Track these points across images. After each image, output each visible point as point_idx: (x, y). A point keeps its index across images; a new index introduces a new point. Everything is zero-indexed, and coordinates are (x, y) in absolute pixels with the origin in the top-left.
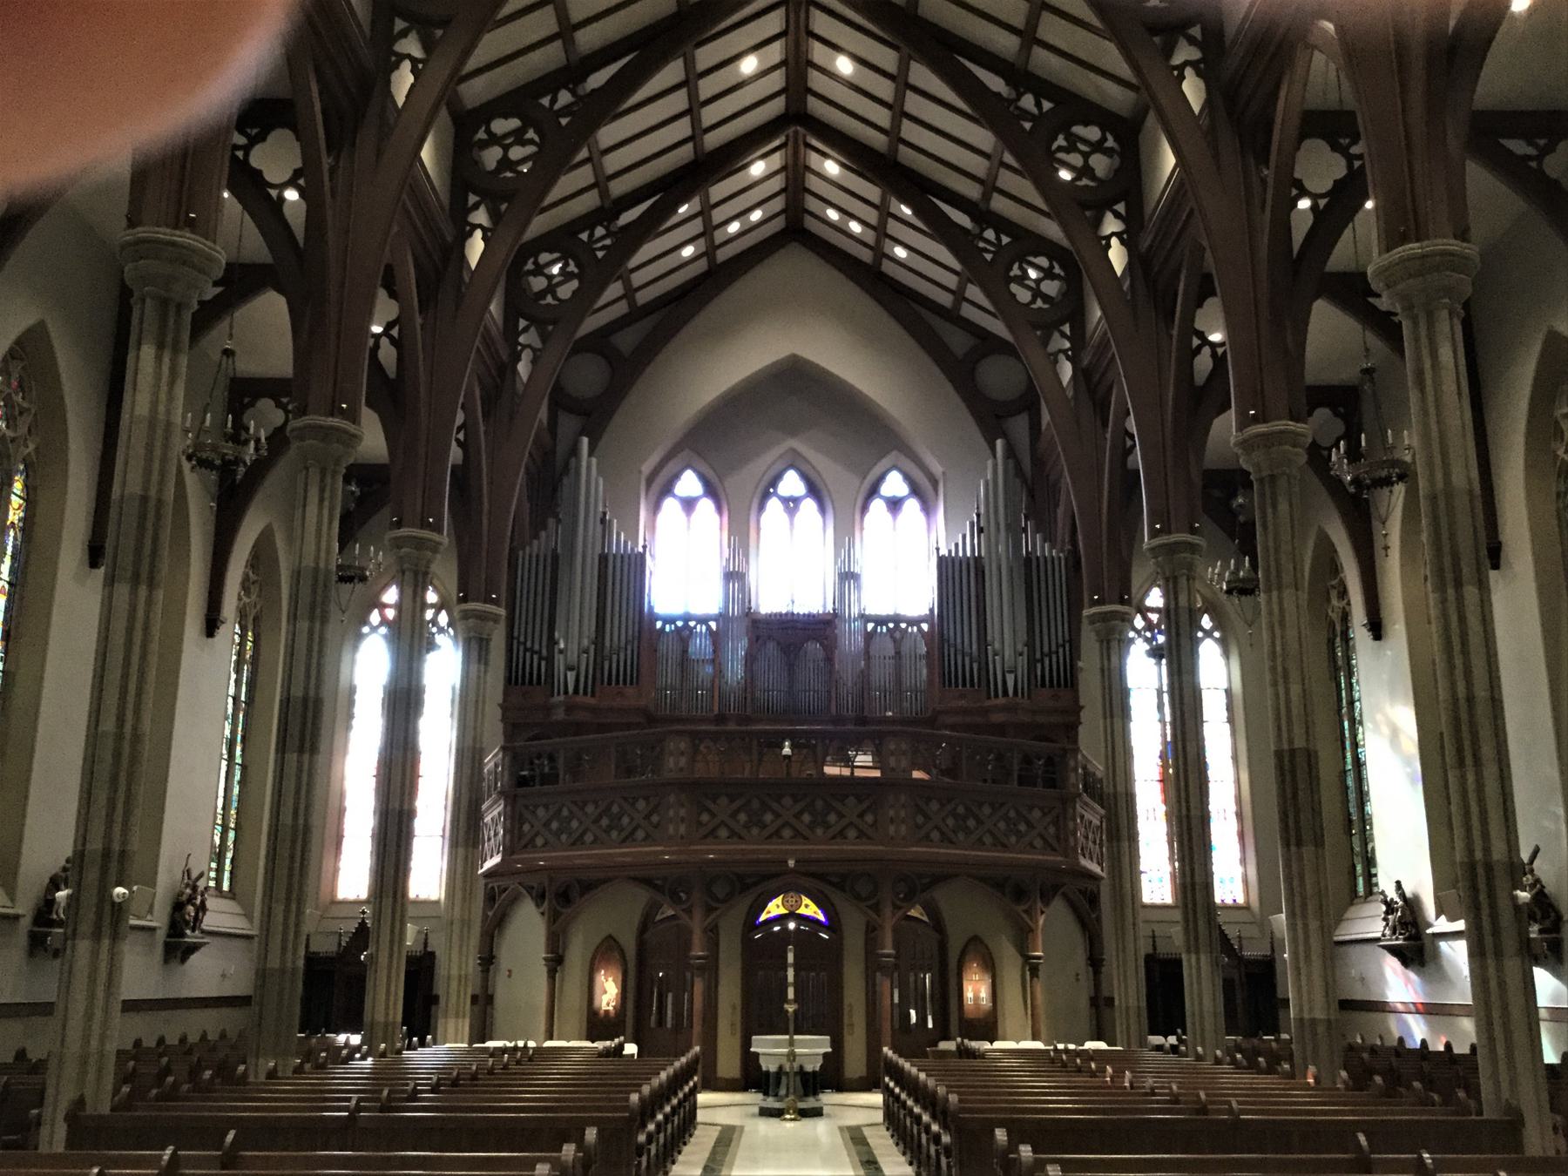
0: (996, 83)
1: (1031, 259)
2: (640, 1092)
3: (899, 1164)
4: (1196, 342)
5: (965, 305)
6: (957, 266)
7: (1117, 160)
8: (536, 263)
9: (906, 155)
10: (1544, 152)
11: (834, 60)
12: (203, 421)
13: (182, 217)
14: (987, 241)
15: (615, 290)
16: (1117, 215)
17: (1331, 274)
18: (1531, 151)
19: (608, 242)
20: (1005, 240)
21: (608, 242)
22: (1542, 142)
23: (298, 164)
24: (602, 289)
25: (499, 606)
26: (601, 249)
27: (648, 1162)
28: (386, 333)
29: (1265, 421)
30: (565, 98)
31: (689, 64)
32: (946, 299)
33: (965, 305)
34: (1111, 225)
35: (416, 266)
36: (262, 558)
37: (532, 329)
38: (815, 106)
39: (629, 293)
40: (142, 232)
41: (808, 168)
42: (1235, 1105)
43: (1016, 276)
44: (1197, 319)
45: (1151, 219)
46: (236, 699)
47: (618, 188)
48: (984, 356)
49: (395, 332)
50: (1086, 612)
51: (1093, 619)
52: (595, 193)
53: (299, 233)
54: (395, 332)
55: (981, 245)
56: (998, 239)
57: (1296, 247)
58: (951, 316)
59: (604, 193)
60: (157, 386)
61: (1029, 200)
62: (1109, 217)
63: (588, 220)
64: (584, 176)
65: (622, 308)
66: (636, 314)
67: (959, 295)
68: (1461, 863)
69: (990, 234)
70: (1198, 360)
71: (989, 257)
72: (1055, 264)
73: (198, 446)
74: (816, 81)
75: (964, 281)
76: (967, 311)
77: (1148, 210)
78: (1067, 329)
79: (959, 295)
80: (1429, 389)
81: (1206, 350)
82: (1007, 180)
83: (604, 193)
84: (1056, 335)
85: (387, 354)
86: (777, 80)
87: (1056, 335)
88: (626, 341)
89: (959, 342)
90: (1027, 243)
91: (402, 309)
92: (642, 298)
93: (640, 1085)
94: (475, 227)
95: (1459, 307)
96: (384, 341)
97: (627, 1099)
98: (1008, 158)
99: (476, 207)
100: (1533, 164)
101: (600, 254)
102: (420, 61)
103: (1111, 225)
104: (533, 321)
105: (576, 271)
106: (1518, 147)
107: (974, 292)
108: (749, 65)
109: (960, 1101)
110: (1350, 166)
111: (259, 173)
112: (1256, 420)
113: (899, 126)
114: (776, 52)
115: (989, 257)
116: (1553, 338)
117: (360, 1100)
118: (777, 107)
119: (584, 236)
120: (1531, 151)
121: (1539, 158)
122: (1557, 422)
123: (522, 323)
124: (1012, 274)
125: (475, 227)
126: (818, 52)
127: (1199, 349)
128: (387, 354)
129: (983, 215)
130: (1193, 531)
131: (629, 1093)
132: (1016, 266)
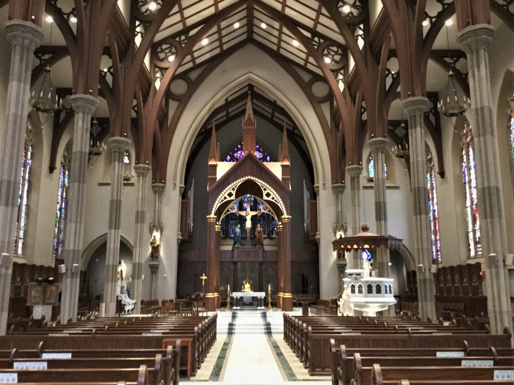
0: (308, 35)
1: (331, 48)
2: (198, 327)
3: (290, 352)
4: (387, 72)
5: (308, 64)
6: (306, 51)
7: (361, 10)
8: (161, 48)
9: (282, 52)
10: (456, 62)
11: (261, 24)
12: (40, 94)
13: (88, 92)
14: (316, 42)
15: (188, 58)
16: (341, 74)
17: (433, 50)
18: (452, 61)
19: (186, 41)
20: (322, 41)
21: (186, 41)
22: (455, 59)
23: (74, 6)
24: (171, 9)
25: (150, 165)
26: (183, 44)
27: (208, 341)
28: (109, 70)
29: (376, 138)
30: (183, 38)
31: (219, 26)
32: (302, 63)
33: (308, 64)
34: (341, 77)
35: (118, 45)
36: (69, 147)
37: (141, 26)
38: (255, 37)
39: (193, 60)
40: (12, 22)
41: (253, 32)
42: (410, 330)
43: (326, 54)
44: (427, 5)
45: (372, 30)
46: (62, 196)
47: (190, 22)
48: (315, 82)
49: (112, 70)
50: (346, 168)
51: (349, 170)
52: (181, 24)
53: (75, 32)
54: (112, 70)
55: (314, 43)
56: (319, 40)
57: (424, 37)
58: (304, 68)
59: (184, 24)
60: (119, 169)
61: (331, 27)
62: (339, 75)
63: (178, 34)
64: (177, 18)
65: (191, 65)
66: (196, 67)
67: (306, 61)
68: (102, 302)
69: (316, 39)
70: (363, 116)
71: (316, 47)
72: (339, 50)
73: (37, 103)
74: (255, 29)
75: (308, 55)
76: (309, 66)
77: (372, 26)
78: (362, 26)
79: (306, 61)
80: (376, 168)
81: (390, 75)
82: (322, 20)
83: (184, 24)
84: (358, 29)
85: (109, 79)
86: (245, 29)
87: (358, 29)
88: (194, 76)
89: (306, 77)
90: (329, 42)
91: (137, 102)
92: (198, 61)
93: (198, 324)
94: (157, 78)
95: (422, 114)
96: (108, 74)
97: (193, 329)
98: (324, 11)
99: (157, 72)
100: (505, 8)
101: (183, 45)
102: (144, 34)
103: (341, 77)
104: (142, 22)
105: (175, 51)
106: (448, 60)
107: (311, 60)
108: (237, 25)
109: (312, 329)
110: (443, 7)
111: (60, 9)
112: (335, 183)
113: (285, 9)
114: (245, 21)
115: (316, 47)
116: (509, 73)
117: (96, 331)
118: (245, 36)
119: (178, 39)
120: (452, 61)
121: (454, 63)
122: (508, 102)
123: (137, 23)
124: (324, 53)
125: (157, 78)
126: (256, 22)
127: (387, 76)
128: (109, 79)
129: (314, 33)
130: (385, 137)
131: (194, 327)
132: (326, 50)
